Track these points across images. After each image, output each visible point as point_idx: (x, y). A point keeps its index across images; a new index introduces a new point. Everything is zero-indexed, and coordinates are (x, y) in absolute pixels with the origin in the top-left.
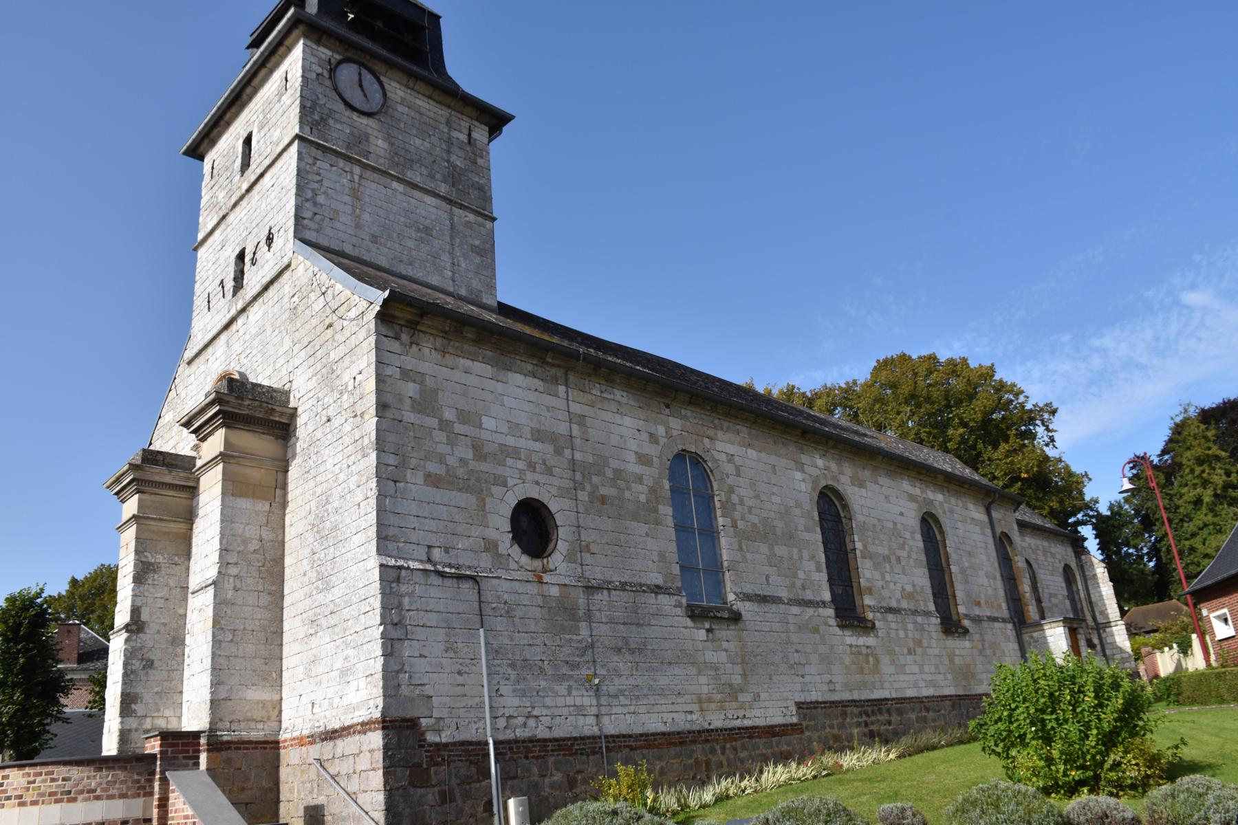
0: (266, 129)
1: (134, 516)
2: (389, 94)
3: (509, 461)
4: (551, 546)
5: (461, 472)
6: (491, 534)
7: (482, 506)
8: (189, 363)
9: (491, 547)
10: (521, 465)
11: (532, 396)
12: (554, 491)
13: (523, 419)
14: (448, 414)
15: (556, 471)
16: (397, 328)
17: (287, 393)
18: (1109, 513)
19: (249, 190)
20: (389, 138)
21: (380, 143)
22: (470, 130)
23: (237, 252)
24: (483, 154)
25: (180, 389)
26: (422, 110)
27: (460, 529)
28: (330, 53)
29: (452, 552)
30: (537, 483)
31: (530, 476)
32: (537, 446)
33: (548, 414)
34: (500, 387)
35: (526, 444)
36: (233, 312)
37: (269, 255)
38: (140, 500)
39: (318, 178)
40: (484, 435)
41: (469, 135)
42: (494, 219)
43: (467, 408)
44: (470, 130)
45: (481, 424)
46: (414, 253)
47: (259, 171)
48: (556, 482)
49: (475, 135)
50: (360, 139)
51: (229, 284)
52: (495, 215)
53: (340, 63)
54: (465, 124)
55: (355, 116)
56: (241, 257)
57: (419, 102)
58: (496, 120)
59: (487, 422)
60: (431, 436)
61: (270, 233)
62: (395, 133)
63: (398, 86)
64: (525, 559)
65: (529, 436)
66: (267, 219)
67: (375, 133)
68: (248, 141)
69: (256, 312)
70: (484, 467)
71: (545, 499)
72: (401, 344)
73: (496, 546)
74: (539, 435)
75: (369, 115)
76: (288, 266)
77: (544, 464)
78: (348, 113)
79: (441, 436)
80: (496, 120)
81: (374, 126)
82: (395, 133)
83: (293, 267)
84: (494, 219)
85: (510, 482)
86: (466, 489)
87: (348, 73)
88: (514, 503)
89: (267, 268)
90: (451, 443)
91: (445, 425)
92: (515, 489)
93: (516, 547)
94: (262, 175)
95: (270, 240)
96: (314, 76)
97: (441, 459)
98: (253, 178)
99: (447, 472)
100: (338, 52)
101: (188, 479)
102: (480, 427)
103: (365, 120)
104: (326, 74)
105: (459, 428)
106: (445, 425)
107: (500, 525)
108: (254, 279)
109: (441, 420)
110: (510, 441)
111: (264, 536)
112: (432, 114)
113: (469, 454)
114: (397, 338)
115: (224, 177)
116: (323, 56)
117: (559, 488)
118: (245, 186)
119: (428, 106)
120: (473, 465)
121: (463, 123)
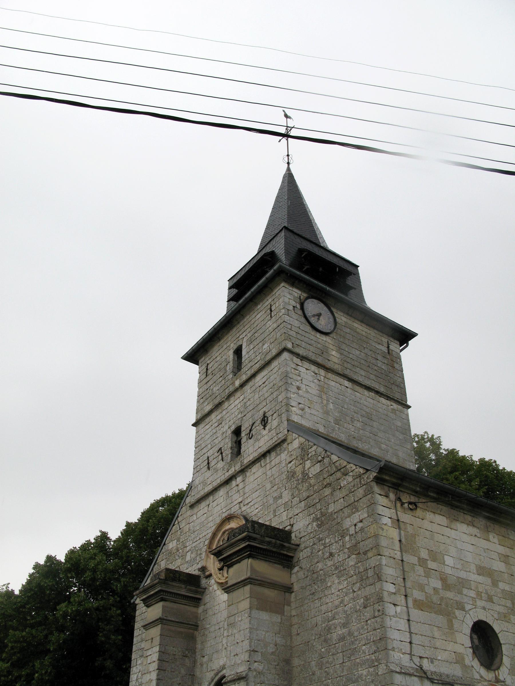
0: (255, 343)
1: (160, 618)
2: (337, 320)
3: (465, 591)
4: (497, 660)
5: (435, 599)
6: (460, 649)
7: (451, 626)
8: (192, 506)
9: (459, 660)
10: (472, 594)
11: (474, 540)
12: (496, 616)
13: (469, 558)
14: (424, 554)
15: (495, 599)
16: (386, 488)
17: (289, 533)
18: (64, 561)
19: (242, 385)
20: (339, 350)
21: (334, 353)
22: (388, 344)
23: (233, 428)
24: (398, 359)
25: (182, 525)
26: (358, 330)
27: (438, 644)
28: (300, 293)
29: (436, 663)
30: (484, 608)
31: (480, 603)
32: (480, 579)
33: (485, 554)
34: (453, 533)
35: (474, 577)
36: (232, 471)
37: (265, 432)
38: (163, 607)
39: (299, 378)
40: (448, 571)
41: (388, 347)
42: (409, 407)
43: (434, 549)
44: (388, 344)
45: (444, 562)
46: (361, 431)
47: (249, 373)
48: (498, 608)
49: (391, 347)
50: (324, 351)
51: (227, 452)
52: (409, 403)
53: (307, 298)
54: (385, 340)
55: (318, 335)
56: (237, 432)
57: (356, 325)
58: (404, 336)
59: (449, 561)
60: (414, 571)
61: (264, 416)
62: (344, 347)
63: (342, 314)
64: (483, 671)
65: (475, 571)
66: (261, 406)
67: (331, 346)
68: (238, 352)
69: (256, 471)
70: (450, 595)
71: (490, 621)
72: (390, 501)
73: (463, 659)
74: (482, 570)
75: (326, 334)
76: (284, 441)
77: (487, 594)
78: (313, 333)
79: (420, 570)
80: (404, 336)
81: (330, 341)
82: (344, 347)
83: (289, 441)
84: (409, 407)
85: (468, 607)
86: (439, 612)
87: (313, 306)
88: (471, 624)
89: (262, 442)
90: (427, 575)
91: (422, 562)
92: (471, 612)
93: (476, 660)
94: (254, 376)
95: (264, 421)
96: (291, 308)
97: (421, 588)
98: (244, 378)
99: (427, 598)
100: (305, 292)
101: (196, 592)
102: (444, 563)
103: (324, 338)
104: (298, 306)
105: (432, 565)
106: (422, 562)
107: (463, 641)
108: (250, 450)
109: (419, 558)
110: (463, 575)
111: (278, 642)
112: (364, 333)
113: (438, 584)
114: (387, 496)
115: (218, 376)
116: (296, 295)
117: (499, 613)
118: (237, 383)
119: (360, 327)
120: (442, 593)
121: (383, 339)
